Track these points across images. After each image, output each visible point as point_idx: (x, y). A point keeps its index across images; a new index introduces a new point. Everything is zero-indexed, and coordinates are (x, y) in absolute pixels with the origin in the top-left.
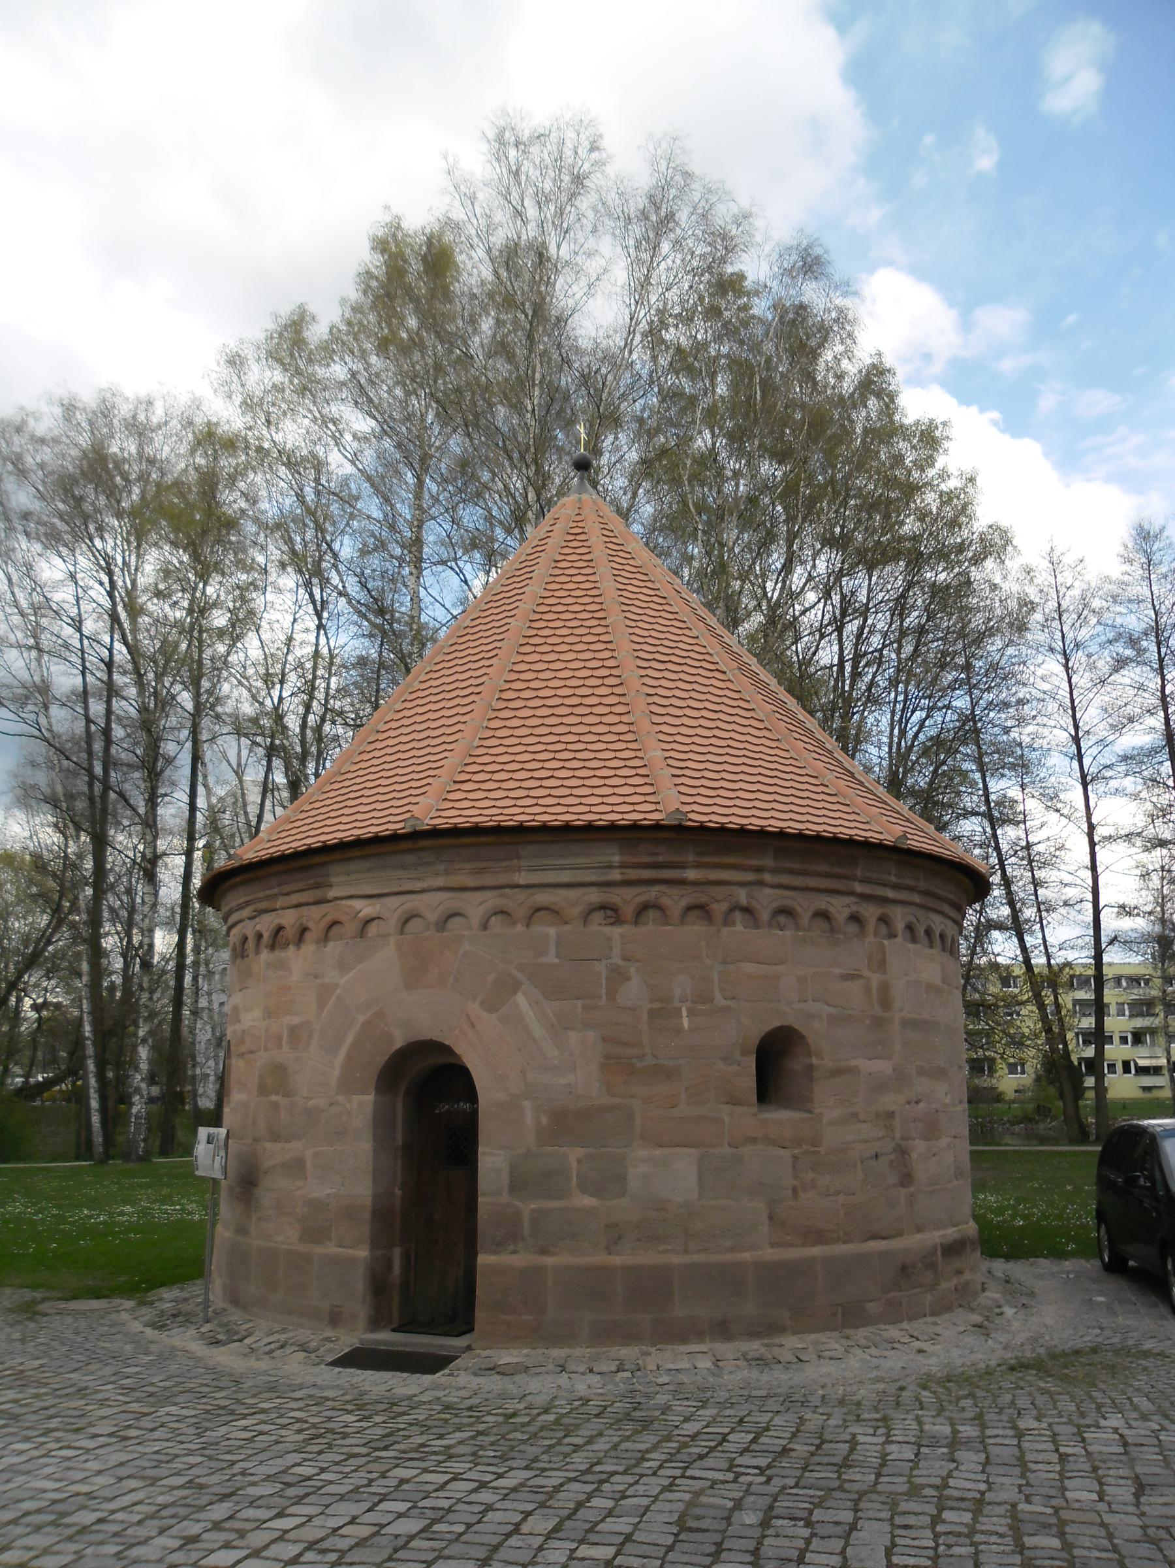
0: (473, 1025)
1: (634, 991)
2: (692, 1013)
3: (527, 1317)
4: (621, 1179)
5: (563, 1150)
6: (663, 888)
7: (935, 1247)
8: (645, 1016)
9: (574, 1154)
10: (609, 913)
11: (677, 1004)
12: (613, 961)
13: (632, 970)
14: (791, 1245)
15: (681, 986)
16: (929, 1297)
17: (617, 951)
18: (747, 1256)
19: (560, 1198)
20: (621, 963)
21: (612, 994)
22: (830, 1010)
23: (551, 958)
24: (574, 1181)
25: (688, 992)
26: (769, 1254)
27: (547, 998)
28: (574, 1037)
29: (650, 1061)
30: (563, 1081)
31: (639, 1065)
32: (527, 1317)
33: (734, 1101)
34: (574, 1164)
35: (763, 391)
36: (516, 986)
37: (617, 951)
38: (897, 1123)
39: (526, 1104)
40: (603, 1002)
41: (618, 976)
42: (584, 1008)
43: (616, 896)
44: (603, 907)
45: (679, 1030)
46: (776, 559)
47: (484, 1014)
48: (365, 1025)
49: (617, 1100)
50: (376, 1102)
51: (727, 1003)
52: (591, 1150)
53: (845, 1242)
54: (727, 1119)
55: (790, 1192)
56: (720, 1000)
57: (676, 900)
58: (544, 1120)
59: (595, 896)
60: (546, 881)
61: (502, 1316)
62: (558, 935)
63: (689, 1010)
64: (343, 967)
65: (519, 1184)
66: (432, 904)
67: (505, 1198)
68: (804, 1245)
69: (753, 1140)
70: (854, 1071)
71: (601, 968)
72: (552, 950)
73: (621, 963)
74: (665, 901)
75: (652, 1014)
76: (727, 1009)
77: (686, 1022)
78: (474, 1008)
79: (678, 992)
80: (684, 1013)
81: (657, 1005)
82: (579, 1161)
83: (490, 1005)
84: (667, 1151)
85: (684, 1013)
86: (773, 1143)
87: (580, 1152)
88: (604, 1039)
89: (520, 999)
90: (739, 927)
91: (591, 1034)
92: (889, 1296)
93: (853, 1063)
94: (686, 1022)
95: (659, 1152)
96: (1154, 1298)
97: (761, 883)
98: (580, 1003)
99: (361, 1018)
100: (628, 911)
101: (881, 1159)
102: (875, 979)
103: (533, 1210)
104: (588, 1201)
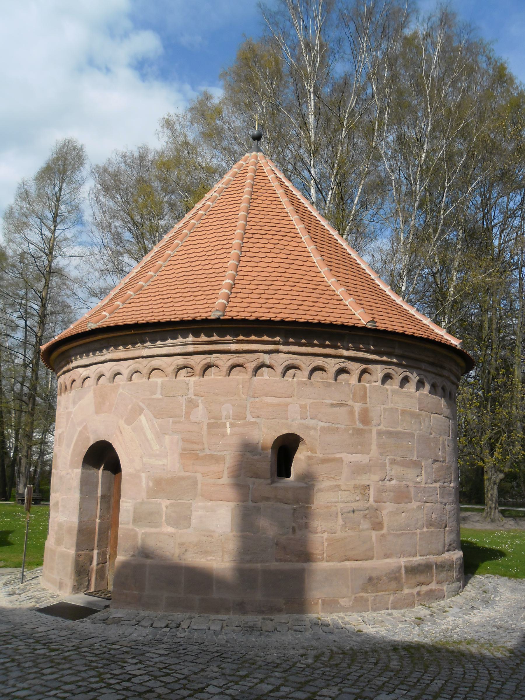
0: (121, 433)
1: (200, 413)
2: (232, 425)
3: (135, 592)
4: (188, 518)
5: (159, 501)
6: (218, 355)
7: (400, 568)
8: (205, 427)
9: (165, 503)
10: (189, 370)
11: (223, 420)
12: (189, 396)
13: (200, 401)
14: (290, 561)
15: (227, 410)
16: (392, 598)
17: (192, 391)
18: (259, 566)
19: (156, 527)
20: (193, 397)
21: (188, 414)
22: (323, 424)
23: (158, 396)
24: (164, 519)
25: (231, 413)
26: (274, 565)
27: (155, 417)
28: (167, 438)
29: (207, 452)
30: (161, 463)
31: (201, 454)
32: (135, 592)
33: (256, 476)
34: (164, 509)
35: (378, 125)
36: (141, 411)
37: (192, 391)
38: (372, 492)
39: (143, 475)
40: (183, 419)
41: (192, 404)
42: (173, 422)
43: (192, 360)
44: (185, 367)
45: (224, 435)
46: (306, 173)
47: (126, 426)
48: (81, 432)
49: (188, 474)
50: (82, 473)
51: (253, 420)
52: (173, 501)
53: (327, 561)
54: (251, 486)
55: (291, 530)
56: (250, 418)
57: (224, 361)
58: (151, 484)
59: (180, 361)
60: (156, 354)
61: (124, 591)
62: (162, 383)
63: (231, 424)
64: (74, 403)
65: (137, 519)
66: (108, 368)
67: (131, 526)
68: (297, 561)
69: (267, 499)
70: (341, 460)
71: (182, 400)
72: (159, 391)
73: (193, 397)
74: (219, 362)
75: (210, 426)
76: (255, 423)
77: (228, 430)
78: (122, 423)
79: (224, 414)
80: (228, 425)
81: (212, 421)
82: (167, 507)
83: (129, 422)
84: (214, 503)
85: (228, 425)
86: (280, 501)
87: (168, 502)
88: (183, 440)
89: (142, 418)
90: (266, 377)
91: (176, 437)
92: (357, 595)
93: (338, 456)
94: (228, 430)
95: (210, 504)
96: (378, 636)
97: (278, 351)
98: (171, 420)
99: (79, 429)
100: (198, 369)
101: (356, 513)
102: (357, 407)
103: (143, 533)
104: (170, 530)
